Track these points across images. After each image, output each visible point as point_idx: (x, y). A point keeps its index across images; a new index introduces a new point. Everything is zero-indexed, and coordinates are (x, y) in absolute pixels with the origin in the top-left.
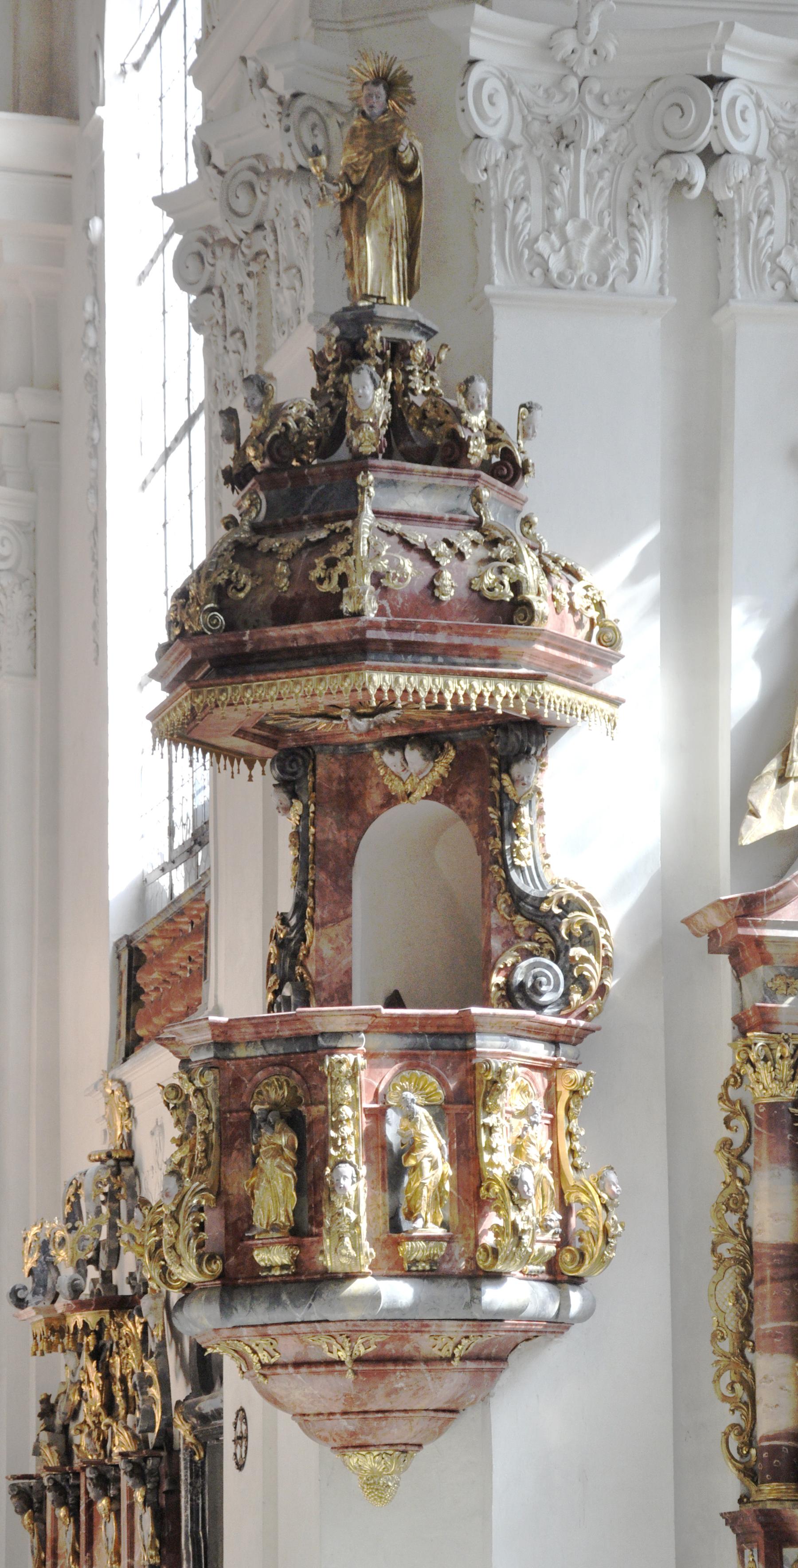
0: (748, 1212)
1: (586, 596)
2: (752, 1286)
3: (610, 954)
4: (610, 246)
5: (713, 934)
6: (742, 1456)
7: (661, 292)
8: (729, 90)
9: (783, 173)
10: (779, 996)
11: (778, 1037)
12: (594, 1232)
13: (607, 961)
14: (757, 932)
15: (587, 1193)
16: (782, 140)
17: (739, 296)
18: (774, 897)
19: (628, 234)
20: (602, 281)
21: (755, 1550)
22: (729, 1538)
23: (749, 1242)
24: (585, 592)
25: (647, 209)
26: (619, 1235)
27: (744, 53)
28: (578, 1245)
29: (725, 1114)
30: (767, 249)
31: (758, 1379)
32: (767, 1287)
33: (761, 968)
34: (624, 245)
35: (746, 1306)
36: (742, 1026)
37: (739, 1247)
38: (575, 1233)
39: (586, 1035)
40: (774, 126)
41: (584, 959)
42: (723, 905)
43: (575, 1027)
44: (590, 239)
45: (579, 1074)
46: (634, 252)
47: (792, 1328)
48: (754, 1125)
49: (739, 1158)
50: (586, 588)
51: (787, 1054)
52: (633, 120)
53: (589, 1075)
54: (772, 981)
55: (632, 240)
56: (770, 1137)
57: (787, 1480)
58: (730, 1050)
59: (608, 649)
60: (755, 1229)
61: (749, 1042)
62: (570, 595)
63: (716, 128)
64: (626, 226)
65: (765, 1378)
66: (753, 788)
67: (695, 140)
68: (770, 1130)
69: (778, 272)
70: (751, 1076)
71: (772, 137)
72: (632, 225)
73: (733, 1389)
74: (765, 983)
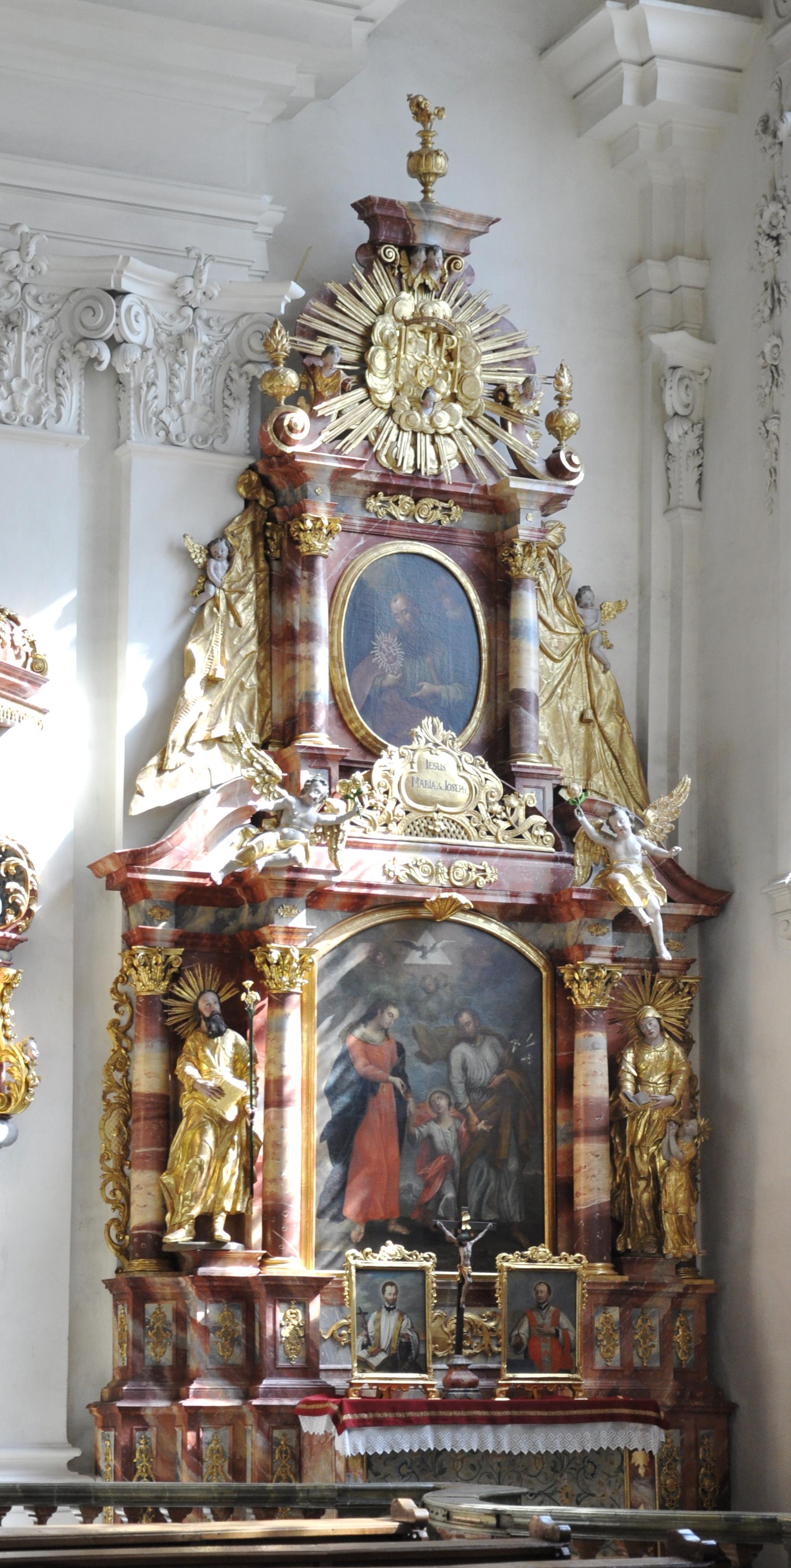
0: (130, 1071)
1: (23, 637)
2: (130, 1123)
3: (35, 888)
4: (43, 398)
5: (110, 876)
6: (119, 1240)
7: (79, 431)
8: (126, 301)
9: (164, 359)
10: (156, 922)
11: (154, 950)
12: (19, 1083)
13: (33, 893)
14: (141, 876)
15: (14, 1055)
16: (163, 337)
17: (133, 438)
18: (154, 852)
19: (56, 390)
20: (37, 421)
21: (126, 1305)
22: (107, 1298)
23: (129, 1092)
24: (22, 634)
25: (69, 374)
26: (36, 1086)
27: (135, 277)
28: (7, 1092)
29: (115, 1002)
30: (153, 409)
31: (132, 1188)
32: (141, 1124)
33: (143, 901)
34: (52, 397)
35: (126, 1136)
36: (128, 941)
37: (122, 1095)
38: (4, 1083)
39: (16, 945)
40: (158, 328)
41: (16, 891)
42: (117, 857)
43: (9, 938)
44: (29, 392)
45: (11, 971)
46: (60, 403)
47: (157, 1152)
48: (136, 1011)
49: (124, 1033)
50: (24, 631)
51: (160, 962)
52: (59, 315)
53: (18, 972)
54: (150, 910)
55: (58, 395)
56: (146, 1019)
57: (151, 1257)
58: (120, 958)
59: (39, 674)
60: (134, 1082)
61: (133, 952)
62: (12, 635)
63: (117, 325)
64: (54, 385)
65: (137, 1186)
66: (140, 776)
67: (102, 332)
68: (146, 1014)
69: (161, 424)
70: (135, 977)
71: (156, 334)
72: (59, 385)
73: (114, 1195)
74: (145, 912)
